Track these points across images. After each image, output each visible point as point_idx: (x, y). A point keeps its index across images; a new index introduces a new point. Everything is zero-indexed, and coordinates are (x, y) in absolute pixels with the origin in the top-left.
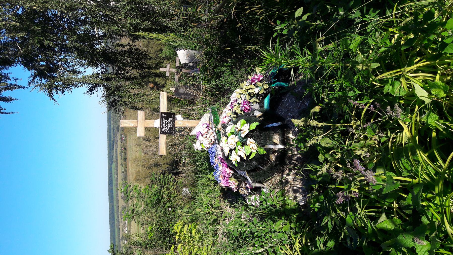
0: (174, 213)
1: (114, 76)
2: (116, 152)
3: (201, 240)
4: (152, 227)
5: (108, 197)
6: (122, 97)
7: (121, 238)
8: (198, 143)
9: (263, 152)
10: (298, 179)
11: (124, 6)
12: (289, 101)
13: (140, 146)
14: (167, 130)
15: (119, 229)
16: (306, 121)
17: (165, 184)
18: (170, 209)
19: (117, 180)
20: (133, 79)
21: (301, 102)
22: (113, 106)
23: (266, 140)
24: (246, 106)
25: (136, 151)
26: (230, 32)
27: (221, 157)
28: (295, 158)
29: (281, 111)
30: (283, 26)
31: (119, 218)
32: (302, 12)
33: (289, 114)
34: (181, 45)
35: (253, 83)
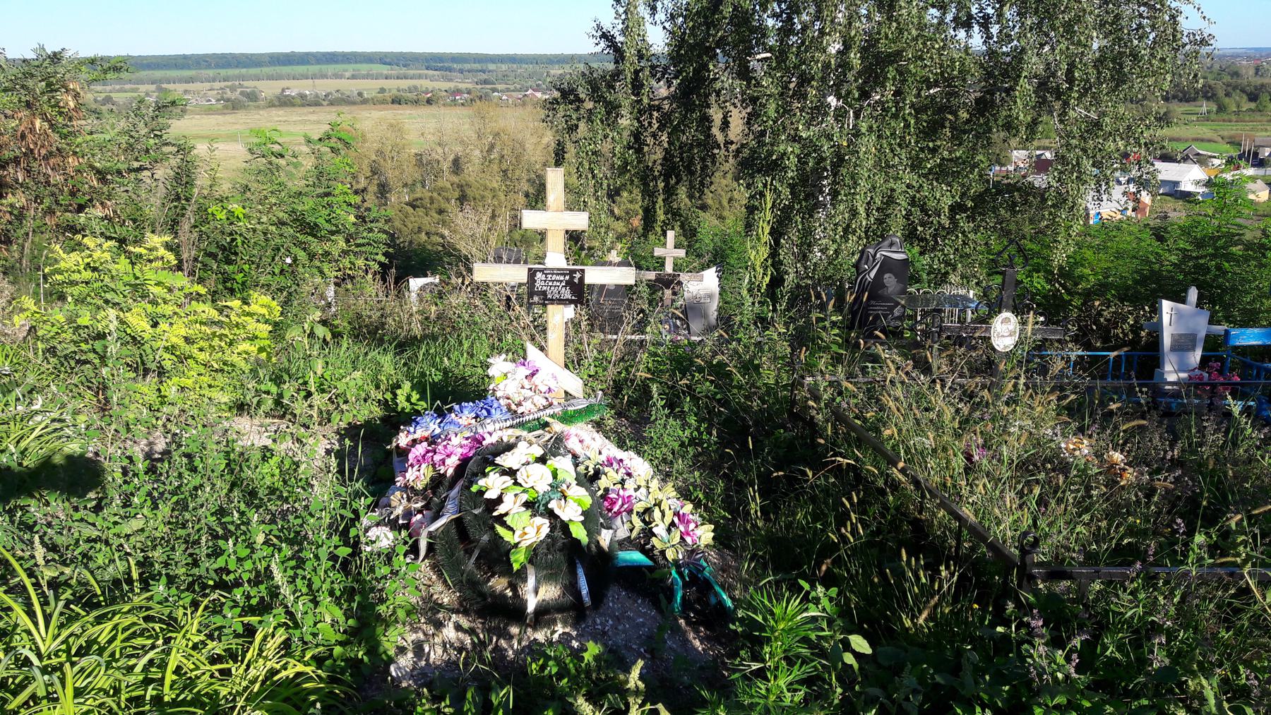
0: (277, 271)
1: (646, 101)
2: (420, 77)
3: (226, 368)
4: (241, 216)
5: (288, 50)
6: (590, 120)
7: (164, 86)
8: (509, 366)
9: (516, 561)
10: (449, 655)
11: (829, 137)
12: (640, 617)
13: (439, 144)
14: (539, 285)
15: (191, 80)
16: (637, 692)
17: (358, 245)
18: (289, 261)
19: (337, 76)
20: (639, 151)
21: (642, 650)
22: (565, 94)
23: (545, 568)
24: (620, 502)
25: (422, 134)
26: (785, 438)
27: (484, 439)
28: (503, 643)
29: (617, 598)
30: (825, 602)
31: (225, 81)
32: (862, 651)
33: (610, 622)
34: (743, 304)
35: (676, 520)
